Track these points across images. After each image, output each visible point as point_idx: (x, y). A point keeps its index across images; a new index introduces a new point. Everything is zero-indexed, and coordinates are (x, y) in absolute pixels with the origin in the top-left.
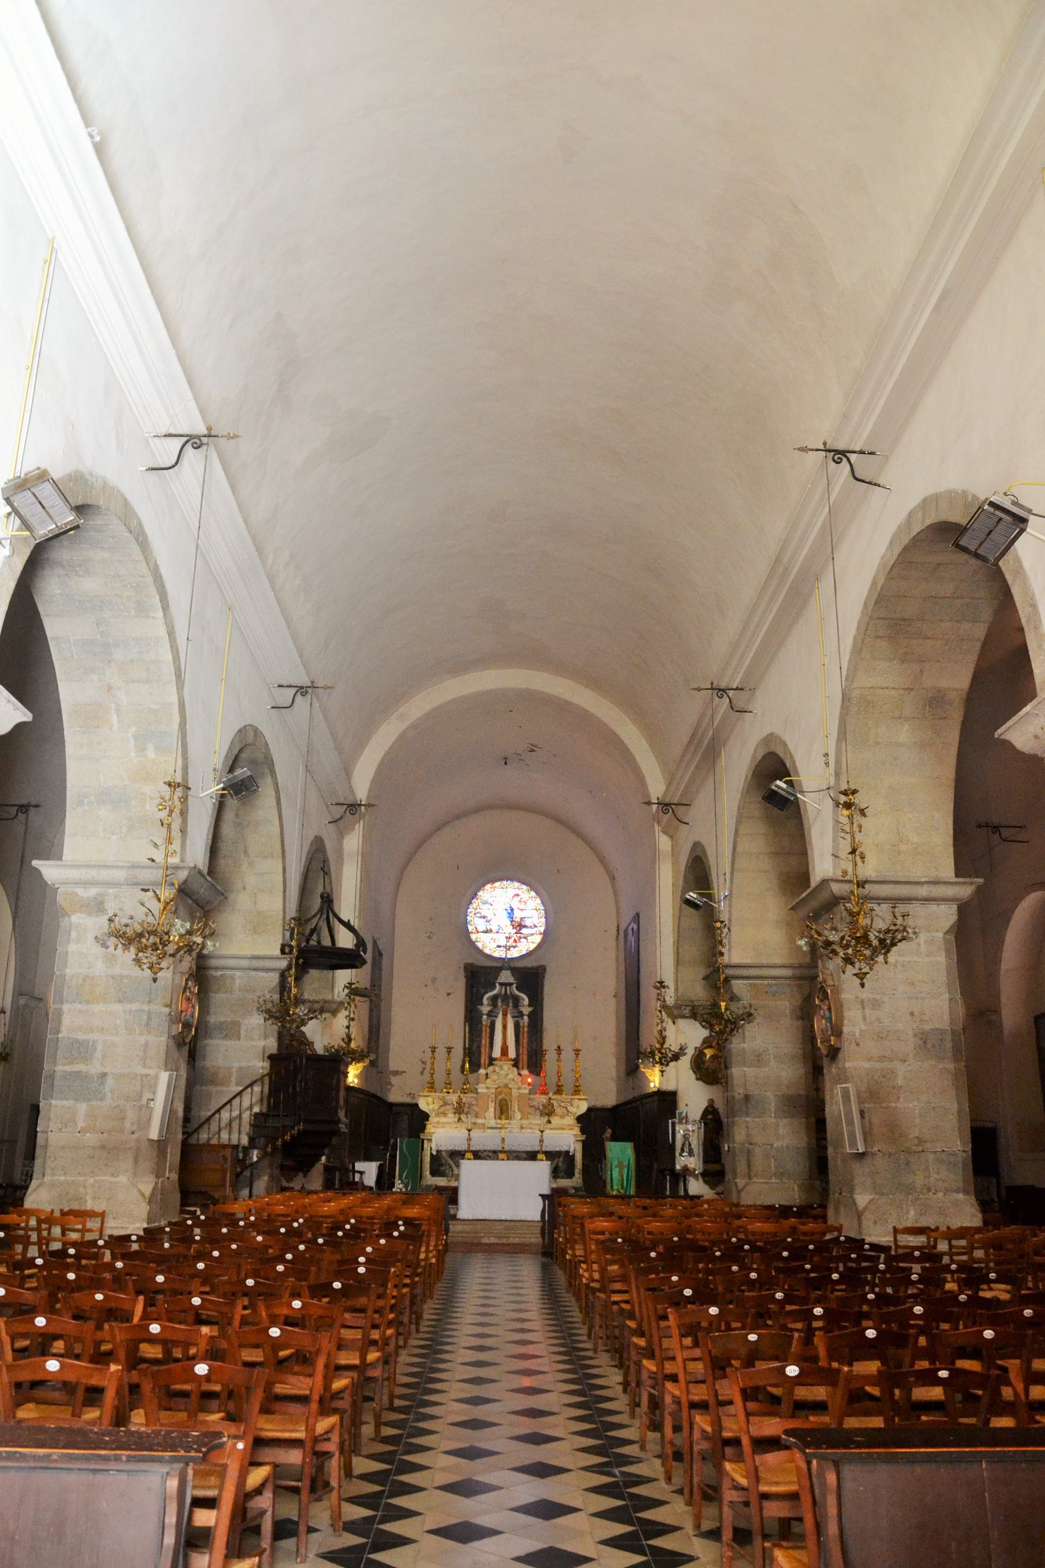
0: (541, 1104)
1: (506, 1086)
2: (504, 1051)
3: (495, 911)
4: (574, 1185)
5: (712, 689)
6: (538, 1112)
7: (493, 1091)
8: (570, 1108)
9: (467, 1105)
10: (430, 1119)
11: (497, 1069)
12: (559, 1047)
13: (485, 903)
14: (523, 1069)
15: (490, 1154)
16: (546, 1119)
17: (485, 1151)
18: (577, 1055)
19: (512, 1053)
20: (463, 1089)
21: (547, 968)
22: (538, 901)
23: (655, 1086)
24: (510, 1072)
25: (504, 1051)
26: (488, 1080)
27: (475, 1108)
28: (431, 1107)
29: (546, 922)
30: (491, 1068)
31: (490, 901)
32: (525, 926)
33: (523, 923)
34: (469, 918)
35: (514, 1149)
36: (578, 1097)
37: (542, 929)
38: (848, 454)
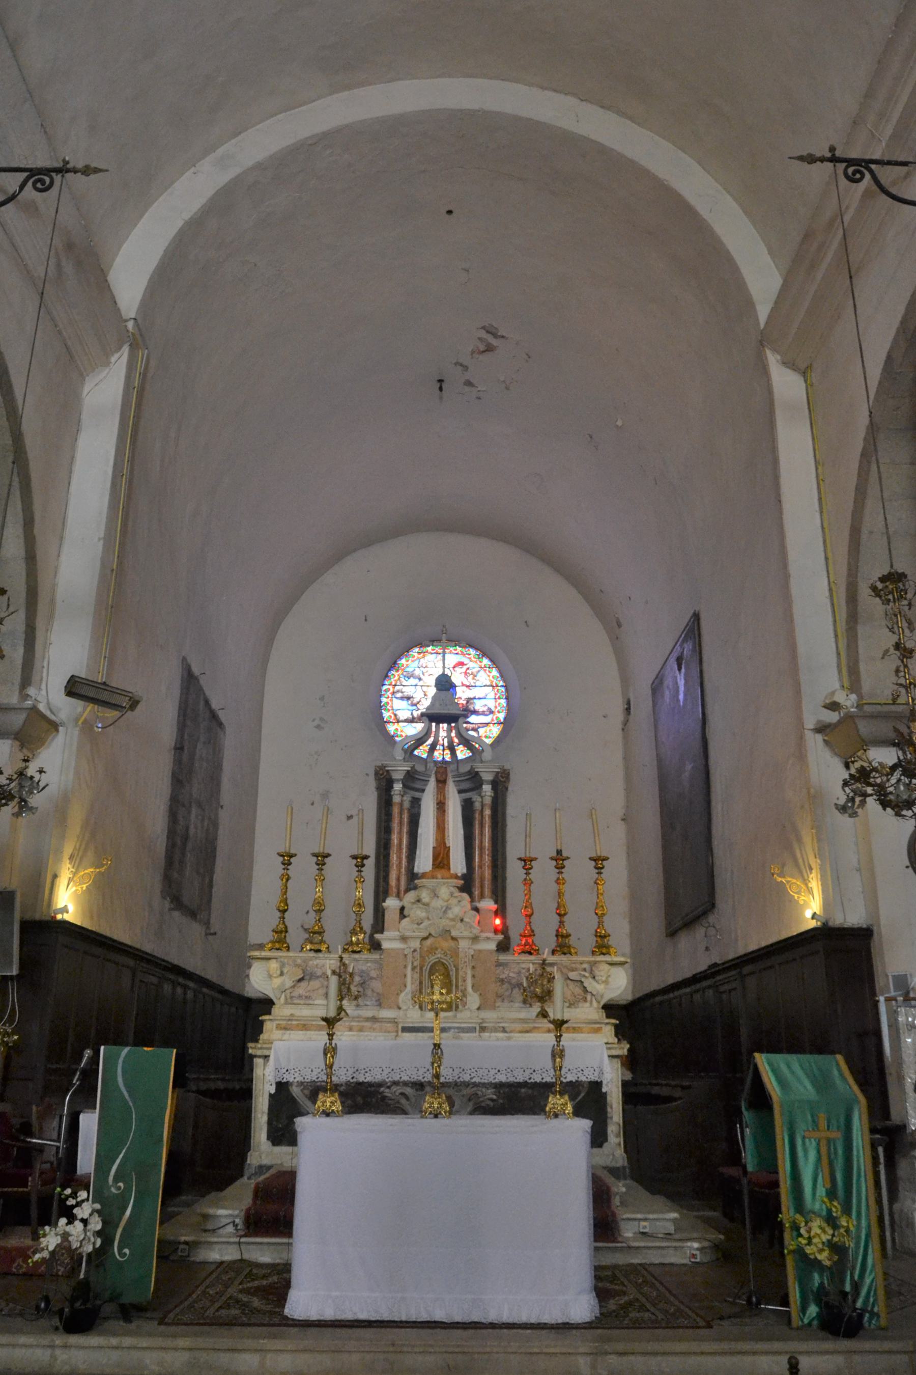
0: (524, 973)
1: (446, 933)
2: (441, 859)
3: (425, 689)
4: (609, 1162)
5: (834, 159)
6: (517, 994)
7: (416, 944)
8: (589, 983)
9: (357, 979)
10: (275, 1010)
11: (425, 896)
12: (559, 852)
13: (410, 676)
14: (482, 896)
15: (408, 1091)
16: (536, 1008)
17: (395, 1083)
18: (599, 869)
19: (458, 864)
20: (351, 943)
21: (512, 776)
22: (495, 672)
23: (814, 916)
24: (454, 901)
25: (441, 859)
26: (405, 921)
27: (376, 985)
28: (277, 982)
29: (508, 705)
30: (411, 896)
31: (418, 672)
32: (475, 712)
33: (471, 707)
34: (384, 700)
35: (466, 1078)
36: (607, 958)
37: (502, 716)
38: (873, 166)
